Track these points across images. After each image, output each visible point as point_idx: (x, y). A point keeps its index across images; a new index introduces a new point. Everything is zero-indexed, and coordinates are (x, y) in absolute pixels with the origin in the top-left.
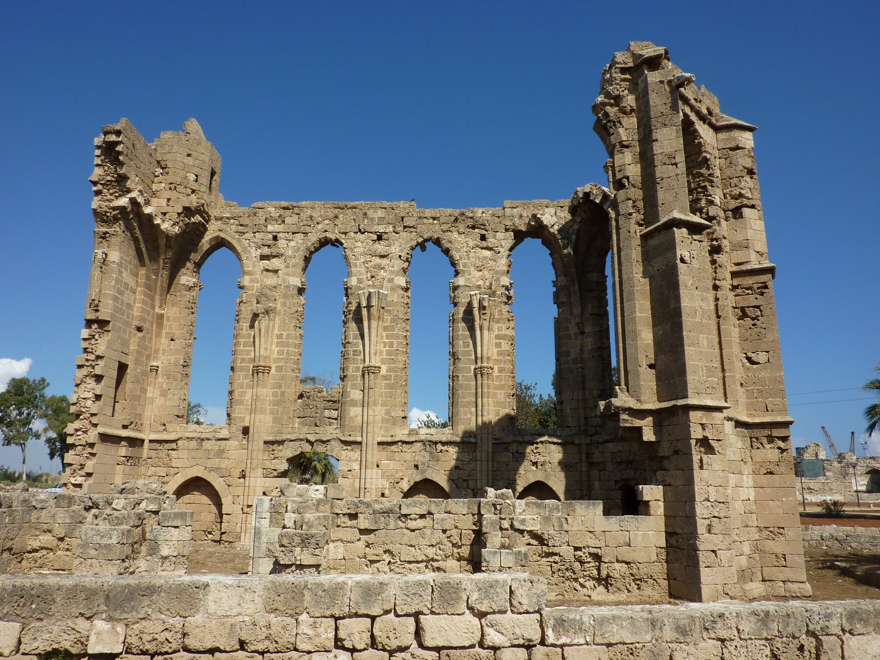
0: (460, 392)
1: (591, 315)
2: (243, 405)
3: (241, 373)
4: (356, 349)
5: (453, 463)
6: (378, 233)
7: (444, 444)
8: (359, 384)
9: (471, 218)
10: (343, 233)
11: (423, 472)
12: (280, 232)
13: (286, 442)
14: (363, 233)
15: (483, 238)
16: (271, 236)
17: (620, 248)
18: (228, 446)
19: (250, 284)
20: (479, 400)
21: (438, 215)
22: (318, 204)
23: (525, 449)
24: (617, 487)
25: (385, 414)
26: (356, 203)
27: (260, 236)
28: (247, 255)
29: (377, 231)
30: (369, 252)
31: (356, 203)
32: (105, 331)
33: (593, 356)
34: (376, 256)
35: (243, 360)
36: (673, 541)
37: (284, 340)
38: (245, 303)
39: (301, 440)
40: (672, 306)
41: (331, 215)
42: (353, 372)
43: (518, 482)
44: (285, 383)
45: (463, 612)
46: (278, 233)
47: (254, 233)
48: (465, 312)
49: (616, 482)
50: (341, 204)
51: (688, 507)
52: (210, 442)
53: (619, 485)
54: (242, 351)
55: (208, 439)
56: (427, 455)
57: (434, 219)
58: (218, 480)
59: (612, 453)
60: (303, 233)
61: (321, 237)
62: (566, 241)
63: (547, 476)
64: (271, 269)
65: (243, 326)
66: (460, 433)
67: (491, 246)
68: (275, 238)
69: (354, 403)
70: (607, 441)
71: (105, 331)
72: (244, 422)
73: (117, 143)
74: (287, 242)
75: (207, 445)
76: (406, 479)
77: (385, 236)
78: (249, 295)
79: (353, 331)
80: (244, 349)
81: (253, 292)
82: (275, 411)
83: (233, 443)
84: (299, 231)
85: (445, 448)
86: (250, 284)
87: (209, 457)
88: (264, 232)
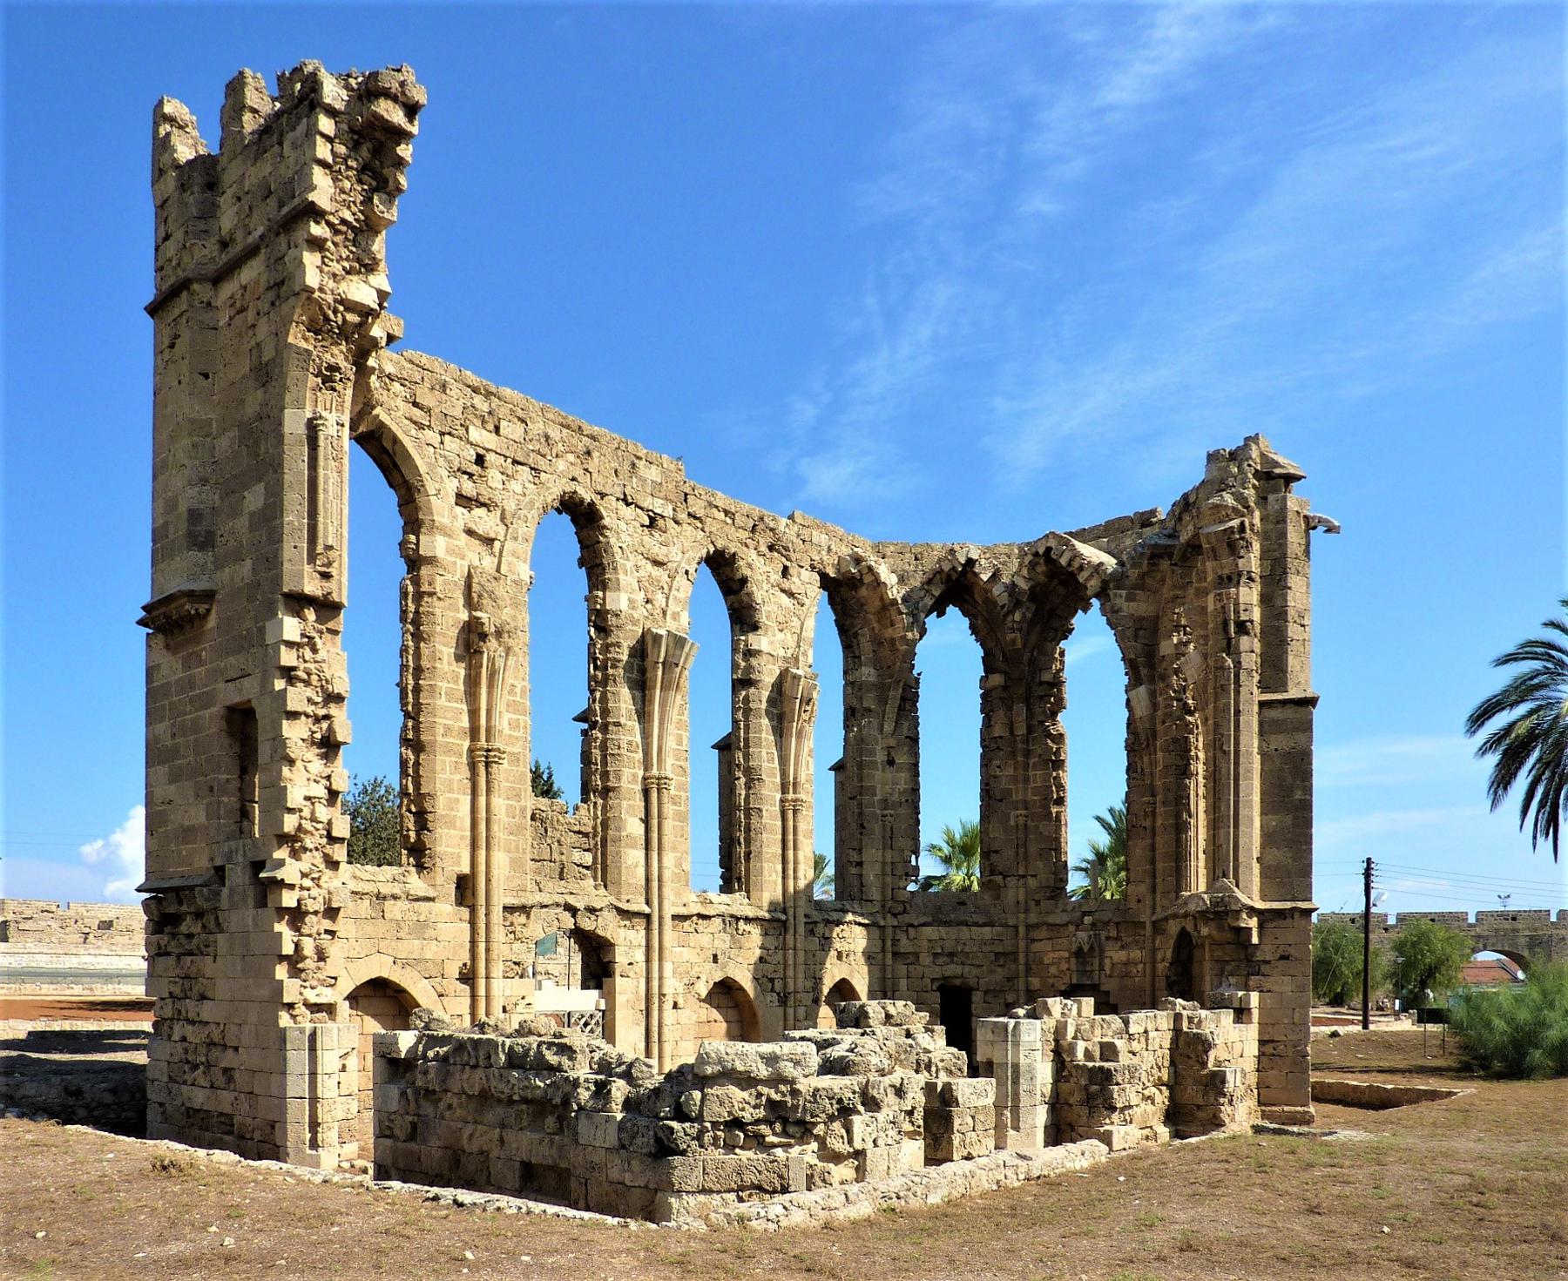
0: (764, 835)
1: (907, 737)
2: (454, 827)
3: (447, 759)
4: (631, 739)
5: (758, 952)
6: (651, 514)
7: (747, 920)
8: (639, 806)
9: (772, 530)
10: (599, 493)
11: (724, 967)
12: (491, 450)
13: (534, 909)
14: (628, 504)
15: (785, 572)
16: (471, 454)
17: (1239, 711)
18: (434, 913)
19: (449, 558)
20: (791, 853)
21: (733, 510)
23: (832, 931)
24: (935, 988)
25: (675, 866)
26: (596, 430)
27: (453, 446)
28: (437, 486)
29: (651, 508)
30: (642, 549)
32: (330, 631)
33: (907, 801)
34: (647, 559)
35: (448, 729)
36: (1269, 1049)
37: (518, 699)
38: (439, 599)
39: (558, 905)
40: (1297, 797)
41: (581, 448)
43: (825, 981)
45: (426, 1203)
46: (488, 450)
47: (442, 434)
48: (770, 701)
49: (933, 980)
52: (399, 903)
54: (446, 709)
55: (395, 897)
56: (727, 938)
57: (726, 512)
58: (420, 986)
59: (930, 941)
60: (532, 469)
61: (568, 489)
62: (911, 620)
63: (851, 972)
64: (480, 532)
65: (441, 652)
66: (765, 905)
67: (794, 591)
68: (480, 460)
70: (924, 925)
71: (330, 631)
72: (458, 864)
73: (401, 135)
75: (394, 909)
77: (660, 522)
79: (625, 702)
80: (448, 704)
81: (456, 579)
82: (514, 843)
84: (526, 461)
85: (748, 928)
86: (449, 558)
88: (461, 439)
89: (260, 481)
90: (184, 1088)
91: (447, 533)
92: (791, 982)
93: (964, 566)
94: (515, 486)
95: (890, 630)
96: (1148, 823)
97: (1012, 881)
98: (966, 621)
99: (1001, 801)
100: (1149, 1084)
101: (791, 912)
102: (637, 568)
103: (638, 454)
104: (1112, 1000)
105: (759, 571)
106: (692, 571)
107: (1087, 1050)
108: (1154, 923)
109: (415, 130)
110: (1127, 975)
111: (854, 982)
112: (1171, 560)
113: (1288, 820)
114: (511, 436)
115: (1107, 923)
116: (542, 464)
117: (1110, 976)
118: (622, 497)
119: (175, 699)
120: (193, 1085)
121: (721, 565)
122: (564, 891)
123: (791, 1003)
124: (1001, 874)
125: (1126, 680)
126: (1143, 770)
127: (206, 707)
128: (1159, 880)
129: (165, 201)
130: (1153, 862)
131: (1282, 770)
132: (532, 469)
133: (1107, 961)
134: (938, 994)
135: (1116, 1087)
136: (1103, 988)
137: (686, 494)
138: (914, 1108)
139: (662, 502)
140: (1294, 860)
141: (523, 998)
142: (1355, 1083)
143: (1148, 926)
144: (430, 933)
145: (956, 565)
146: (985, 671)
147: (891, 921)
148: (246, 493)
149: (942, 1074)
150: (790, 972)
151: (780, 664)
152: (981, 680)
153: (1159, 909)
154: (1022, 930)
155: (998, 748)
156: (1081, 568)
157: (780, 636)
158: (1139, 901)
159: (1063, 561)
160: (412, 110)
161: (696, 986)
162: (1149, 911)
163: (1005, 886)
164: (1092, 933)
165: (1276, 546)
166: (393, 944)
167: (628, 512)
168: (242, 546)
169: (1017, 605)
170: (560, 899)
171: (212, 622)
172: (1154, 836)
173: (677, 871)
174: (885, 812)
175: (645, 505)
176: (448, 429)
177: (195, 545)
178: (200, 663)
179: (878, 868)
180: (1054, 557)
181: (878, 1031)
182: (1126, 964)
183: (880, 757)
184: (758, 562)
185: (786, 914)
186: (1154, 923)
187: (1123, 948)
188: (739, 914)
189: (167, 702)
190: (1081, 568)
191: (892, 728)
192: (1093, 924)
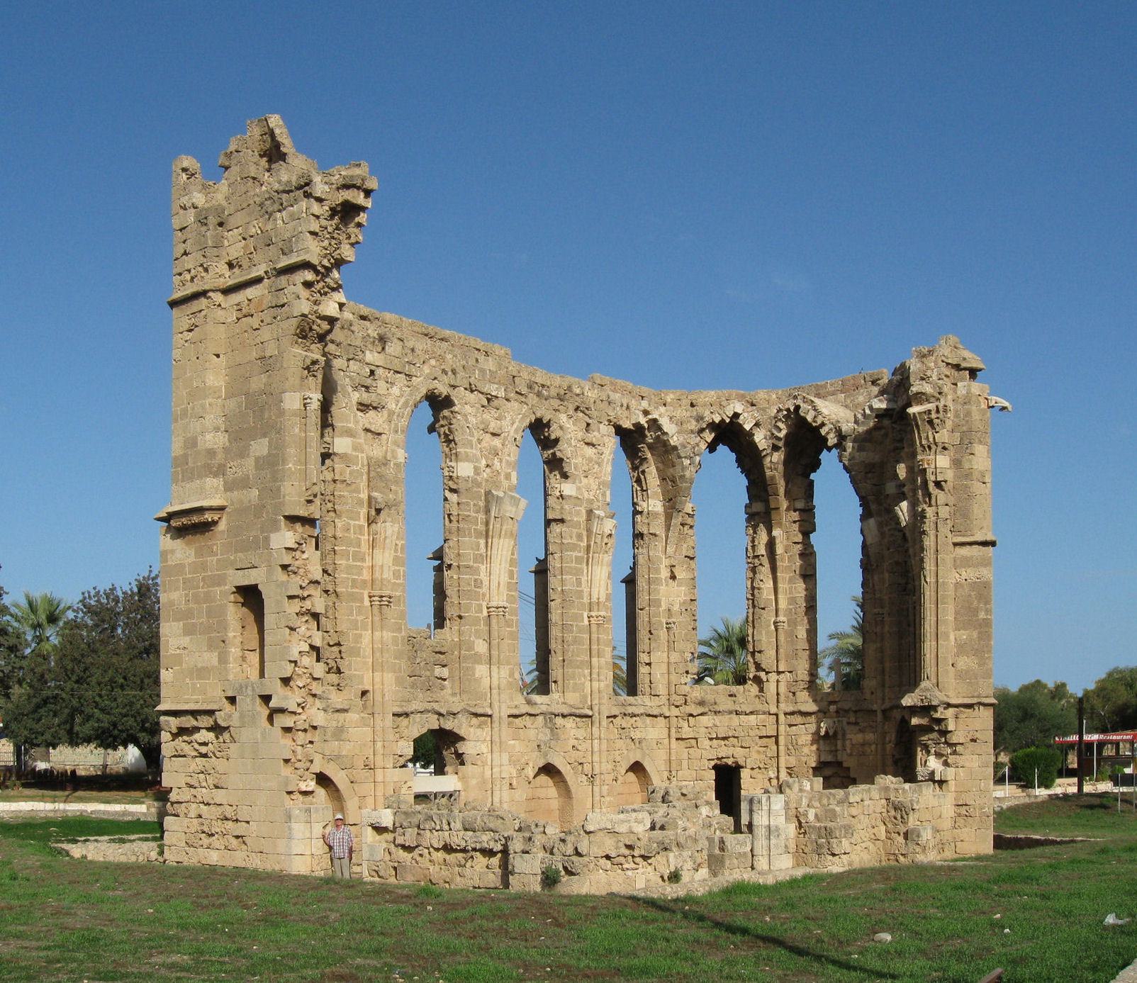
14: (472, 391)
19: (354, 453)
21: (549, 384)
26: (447, 333)
31: (447, 333)
42: (476, 612)
44: (405, 624)
46: (377, 366)
50: (431, 329)
51: (983, 784)
53: (713, 763)
56: (548, 731)
58: (340, 775)
60: (406, 375)
63: (644, 755)
68: (372, 372)
69: (477, 659)
74: (389, 386)
76: (531, 765)
78: (354, 470)
82: (398, 666)
83: (353, 716)
86: (354, 453)
87: (325, 738)
89: (264, 435)
90: (200, 850)
91: (349, 433)
92: (596, 766)
93: (731, 418)
94: (395, 391)
95: (671, 470)
96: (878, 629)
97: (773, 677)
98: (733, 456)
99: (763, 609)
100: (865, 839)
101: (596, 708)
102: (480, 441)
103: (478, 347)
104: (852, 775)
105: (567, 428)
106: (518, 438)
107: (816, 815)
108: (884, 711)
109: (369, 205)
110: (864, 754)
111: (544, 697)
112: (891, 419)
113: (975, 634)
114: (393, 354)
115: (847, 711)
116: (413, 370)
117: (851, 755)
118: (468, 386)
120: (208, 848)
121: (538, 429)
122: (430, 699)
123: (597, 782)
124: (764, 670)
125: (860, 511)
126: (874, 585)
127: (219, 585)
128: (887, 677)
129: (184, 228)
130: (882, 662)
131: (970, 595)
132: (406, 375)
133: (848, 742)
134: (713, 772)
135: (835, 840)
136: (845, 765)
137: (514, 377)
138: (702, 849)
139: (496, 386)
140: (979, 666)
141: (406, 782)
142: (1038, 837)
143: (879, 715)
144: (344, 736)
145: (725, 418)
146: (750, 498)
147: (675, 712)
148: (252, 443)
149: (718, 832)
150: (596, 758)
151: (585, 505)
153: (887, 701)
154: (782, 717)
155: (761, 564)
156: (823, 424)
157: (585, 481)
158: (872, 693)
159: (809, 418)
160: (368, 193)
161: (526, 771)
162: (879, 701)
163: (767, 681)
164: (836, 720)
165: (964, 422)
166: (322, 745)
167: (473, 397)
168: (249, 478)
169: (775, 448)
170: (429, 706)
171: (222, 526)
172: (882, 640)
173: (510, 680)
174: (670, 621)
175: (485, 390)
176: (351, 357)
177: (211, 473)
178: (213, 553)
179: (664, 668)
180: (802, 414)
181: (677, 805)
182: (863, 745)
183: (665, 573)
184: (568, 425)
185: (592, 709)
186: (884, 711)
187: (861, 731)
188: (556, 712)
189: (181, 578)
190: (823, 424)
191: (674, 550)
192: (837, 712)
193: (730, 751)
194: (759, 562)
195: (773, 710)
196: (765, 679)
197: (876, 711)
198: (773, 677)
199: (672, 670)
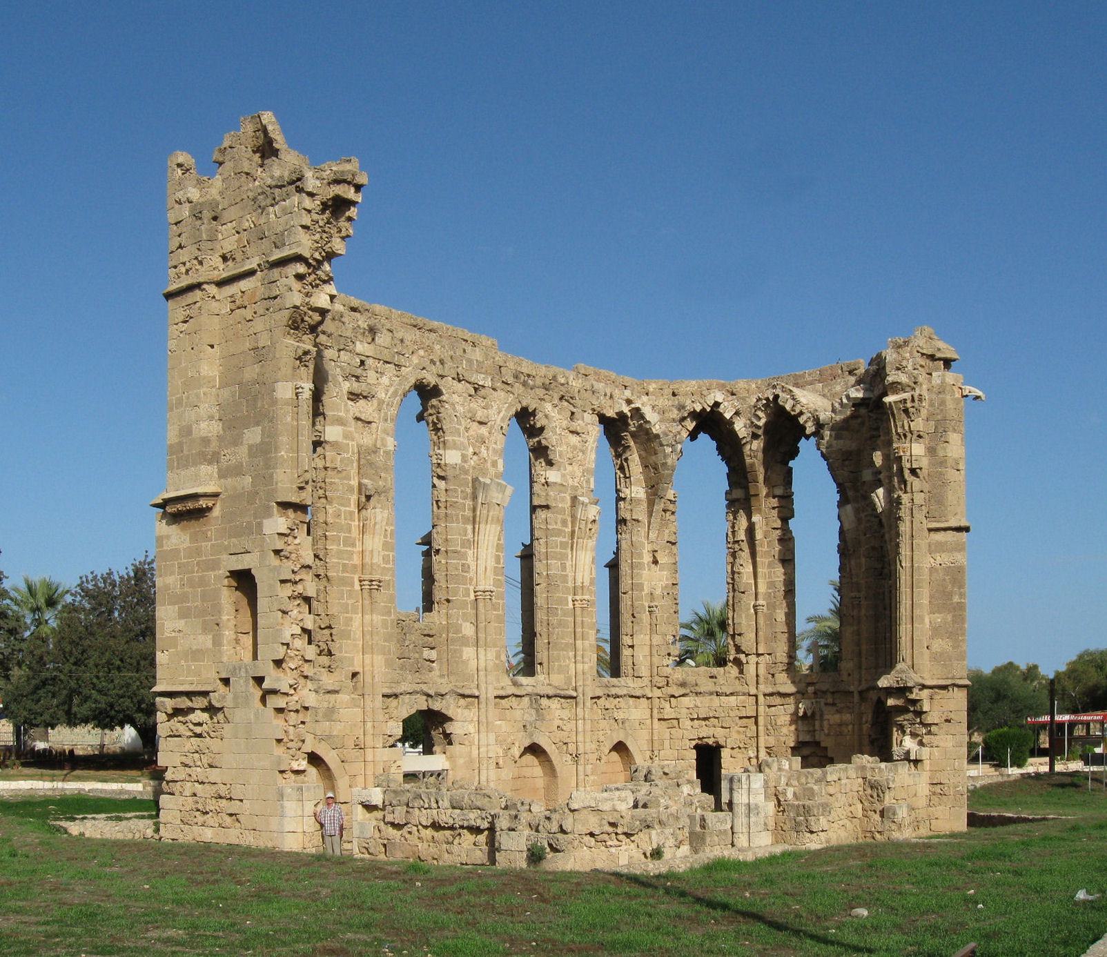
14: (460, 381)
19: (345, 441)
21: (534, 374)
22: (486, 341)
26: (435, 324)
31: (435, 324)
42: (463, 596)
44: (394, 608)
50: (420, 321)
51: (957, 763)
53: (694, 743)
56: (533, 712)
58: (331, 755)
60: (395, 365)
63: (627, 735)
68: (362, 363)
69: (464, 641)
74: (379, 375)
76: (517, 745)
78: (344, 458)
82: (387, 649)
83: (343, 697)
86: (345, 441)
87: (317, 718)
89: (257, 424)
90: (195, 827)
91: (340, 422)
92: (581, 745)
93: (712, 407)
94: (385, 380)
95: (653, 458)
96: (855, 613)
97: (753, 659)
98: (714, 444)
99: (743, 593)
100: (842, 817)
101: (580, 690)
102: (467, 429)
103: (465, 338)
105: (552, 416)
106: (505, 426)
107: (795, 794)
108: (860, 693)
109: (360, 200)
110: (841, 734)
112: (868, 408)
113: (949, 618)
114: (383, 345)
115: (824, 692)
116: (402, 361)
117: (828, 735)
118: (456, 376)
119: (183, 561)
120: (203, 825)
121: (524, 417)
122: (419, 681)
123: (582, 761)
124: (744, 652)
125: (837, 497)
126: (850, 570)
127: (213, 569)
128: (863, 659)
129: (179, 222)
130: (858, 644)
131: (944, 580)
132: (395, 365)
133: (825, 723)
134: (694, 751)
135: (813, 818)
136: (823, 744)
137: (500, 367)
138: (684, 826)
139: (483, 376)
140: (953, 648)
141: (395, 761)
143: (856, 696)
144: (335, 716)
145: (706, 407)
146: (730, 485)
147: (658, 693)
148: (245, 431)
149: (699, 810)
150: (580, 738)
151: (569, 492)
152: (726, 493)
153: (864, 682)
154: (761, 698)
155: (741, 549)
156: (801, 413)
157: (569, 468)
158: (849, 675)
159: (788, 407)
160: (358, 188)
161: (512, 750)
162: (856, 683)
163: (747, 663)
164: (814, 701)
165: (938, 411)
166: (313, 725)
167: (460, 387)
168: (242, 466)
169: (755, 436)
171: (216, 512)
172: (859, 623)
173: (497, 662)
174: (652, 604)
175: (472, 380)
177: (205, 461)
178: (207, 539)
179: (646, 650)
180: (781, 403)
181: (659, 784)
182: (840, 725)
183: (647, 558)
184: (553, 413)
185: (576, 690)
186: (860, 693)
187: (838, 712)
188: (542, 693)
189: (176, 563)
190: (801, 413)
191: (656, 535)
192: (815, 693)
193: (710, 731)
194: (739, 548)
195: (753, 691)
196: (744, 661)
197: (853, 692)
198: (753, 659)
199: (654, 652)
